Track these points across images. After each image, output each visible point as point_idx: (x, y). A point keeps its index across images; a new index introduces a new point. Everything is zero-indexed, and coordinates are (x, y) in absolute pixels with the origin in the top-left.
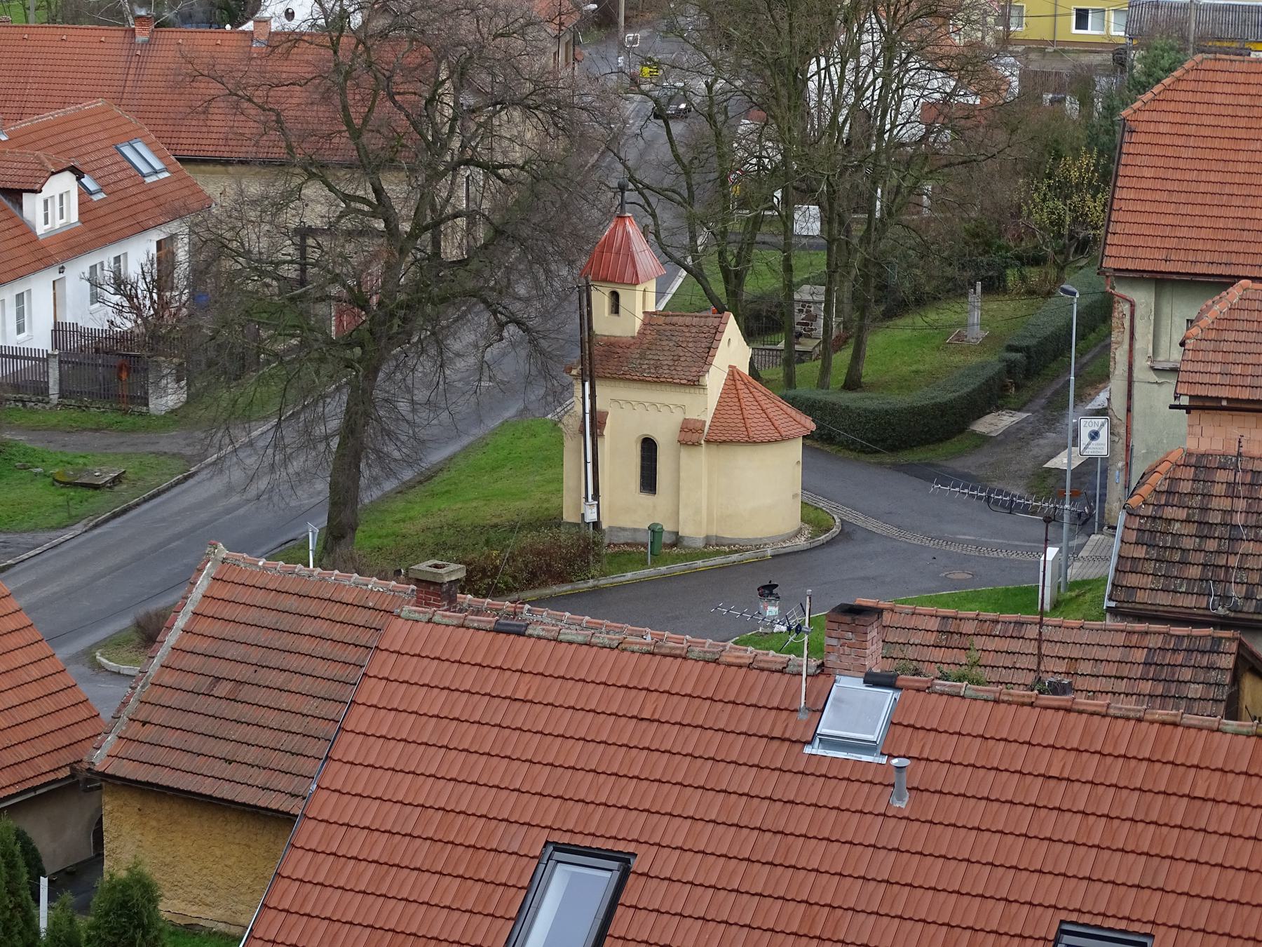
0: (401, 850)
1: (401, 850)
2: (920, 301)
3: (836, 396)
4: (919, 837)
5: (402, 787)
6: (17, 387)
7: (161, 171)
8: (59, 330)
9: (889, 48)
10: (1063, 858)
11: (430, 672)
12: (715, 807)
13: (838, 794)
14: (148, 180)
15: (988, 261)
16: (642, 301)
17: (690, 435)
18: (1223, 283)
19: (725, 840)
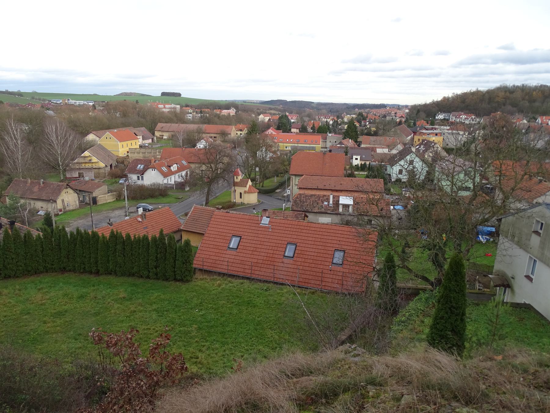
0: (216, 236)
1: (216, 236)
2: (270, 178)
3: (261, 188)
4: (272, 234)
5: (216, 230)
8: (175, 181)
9: (266, 150)
10: (288, 236)
11: (219, 217)
12: (250, 231)
13: (264, 229)
15: (277, 173)
16: (240, 178)
17: (245, 192)
18: (302, 175)
19: (252, 235)
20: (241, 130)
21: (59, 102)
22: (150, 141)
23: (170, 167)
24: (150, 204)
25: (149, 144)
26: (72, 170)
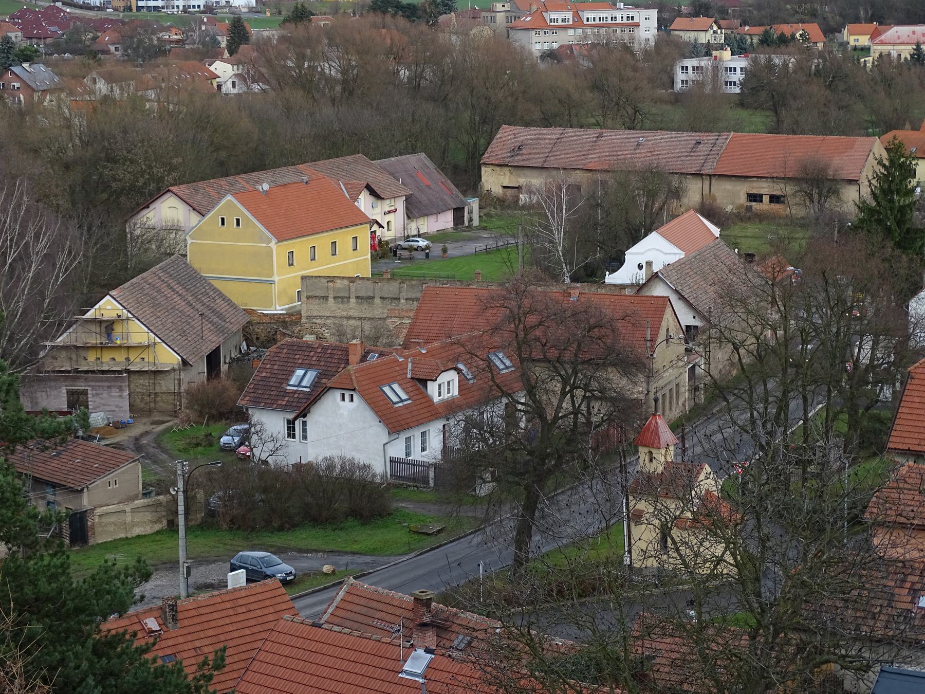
6: (414, 480)
7: (406, 400)
14: (397, 405)
22: (446, 221)
23: (424, 382)
24: (278, 551)
25: (440, 237)
26: (45, 378)
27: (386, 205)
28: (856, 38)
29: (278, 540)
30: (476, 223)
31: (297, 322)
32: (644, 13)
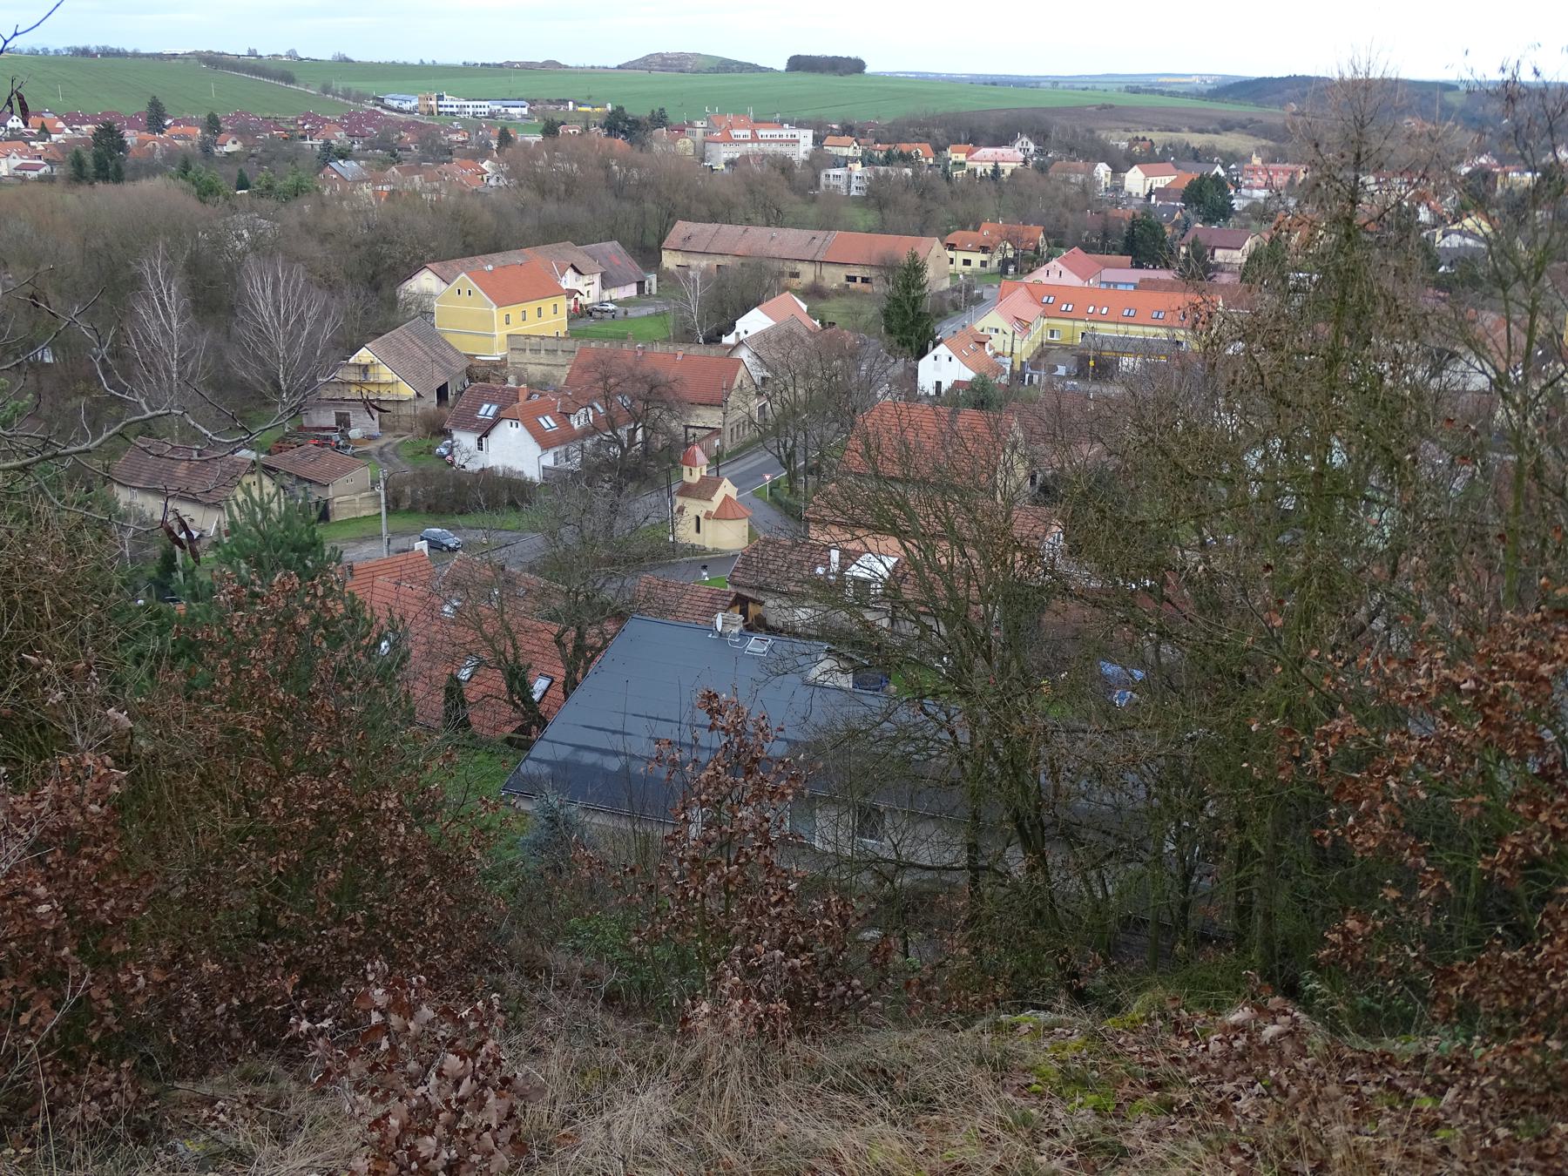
17: (708, 515)
20: (984, 250)
21: (406, 106)
22: (631, 291)
23: (568, 415)
24: (455, 529)
25: (627, 302)
27: (586, 279)
28: (955, 155)
29: (459, 520)
30: (654, 291)
31: (505, 366)
32: (804, 132)
